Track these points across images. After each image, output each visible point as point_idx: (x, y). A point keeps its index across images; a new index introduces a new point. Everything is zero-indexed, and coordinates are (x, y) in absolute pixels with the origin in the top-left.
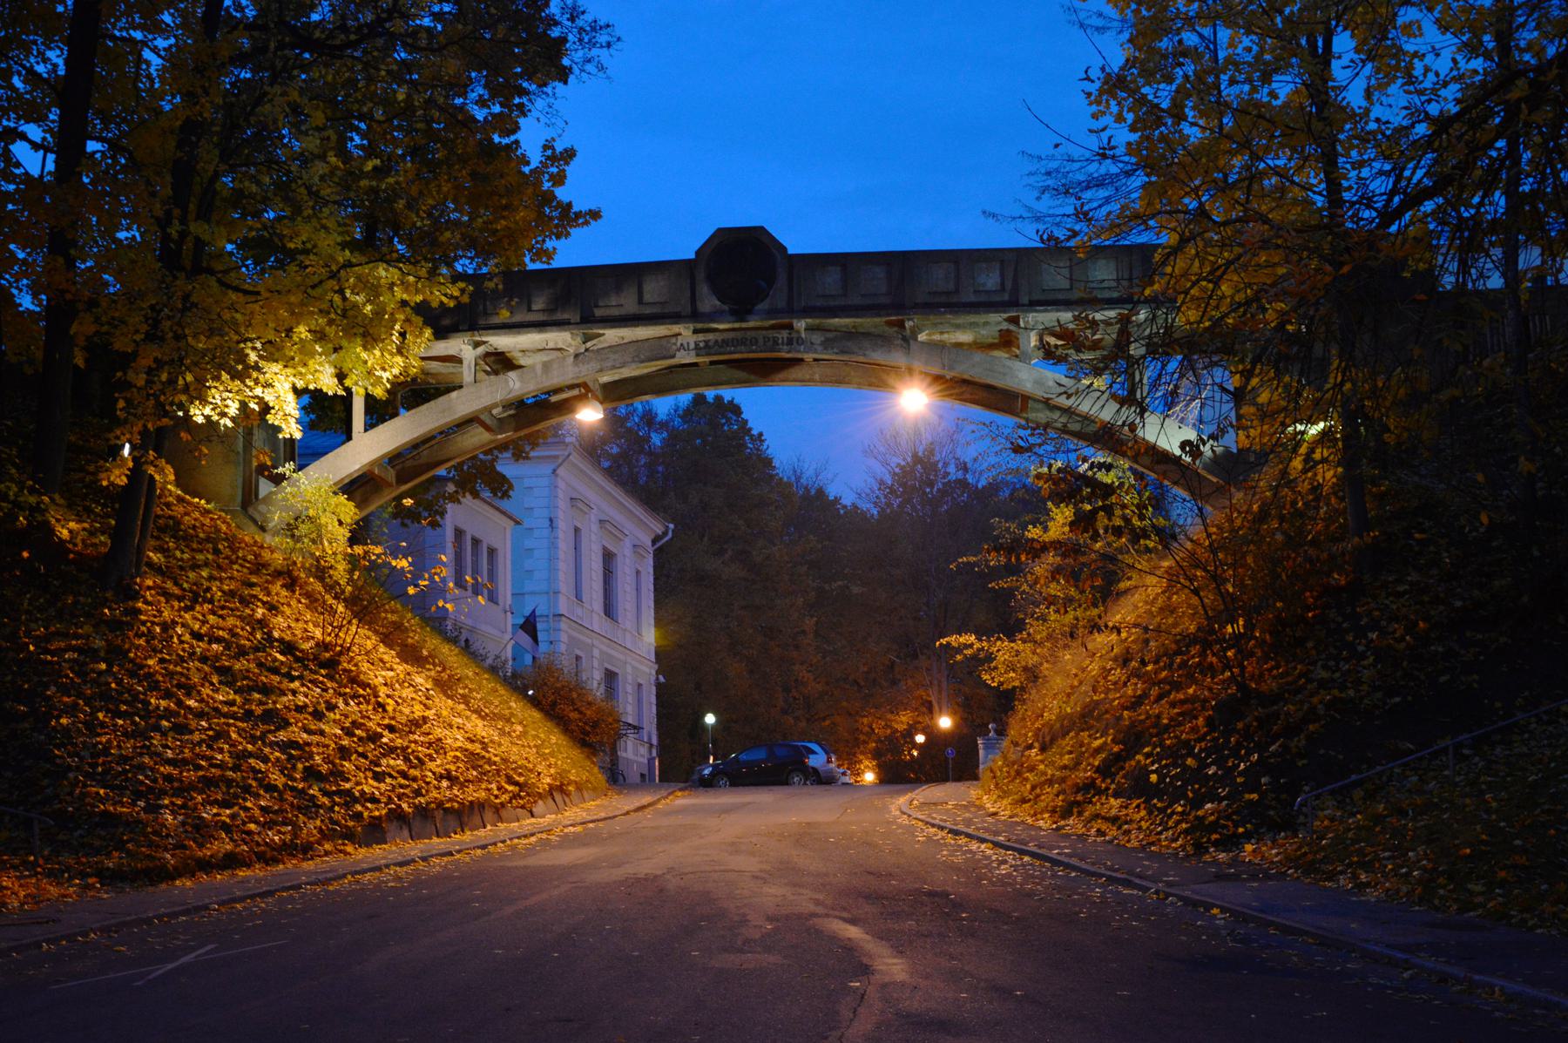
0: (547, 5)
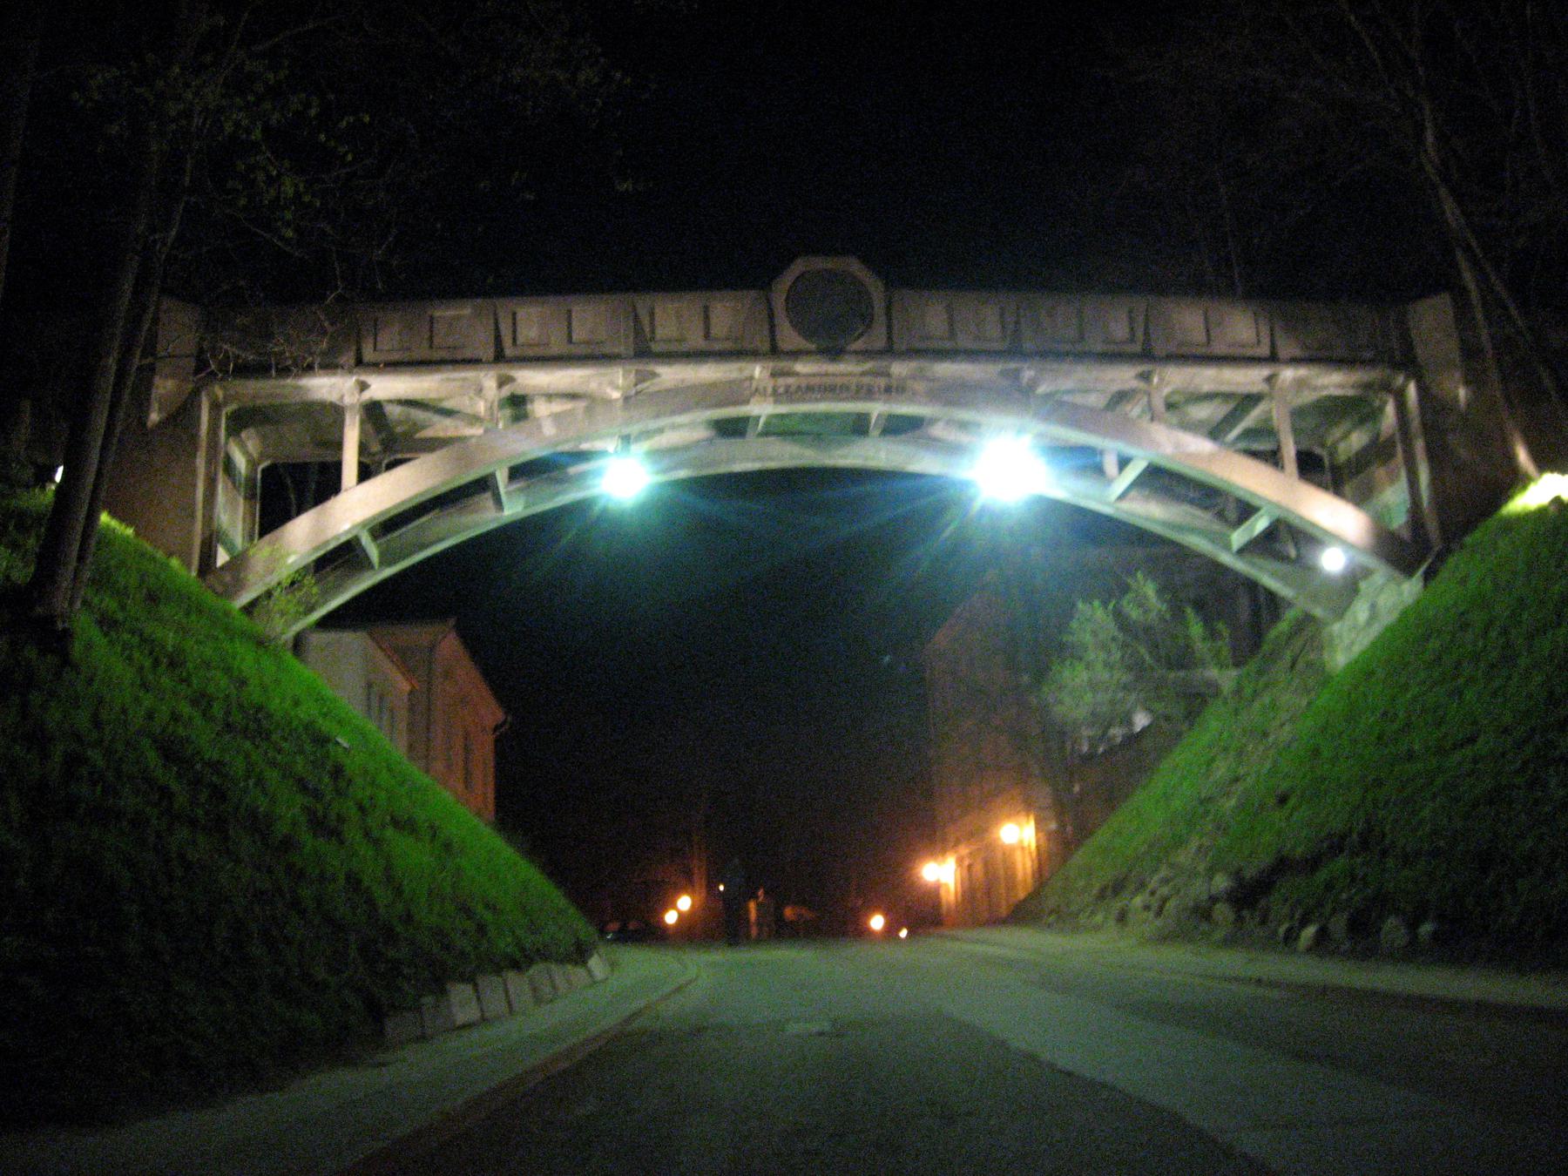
0: (1548, 460)
